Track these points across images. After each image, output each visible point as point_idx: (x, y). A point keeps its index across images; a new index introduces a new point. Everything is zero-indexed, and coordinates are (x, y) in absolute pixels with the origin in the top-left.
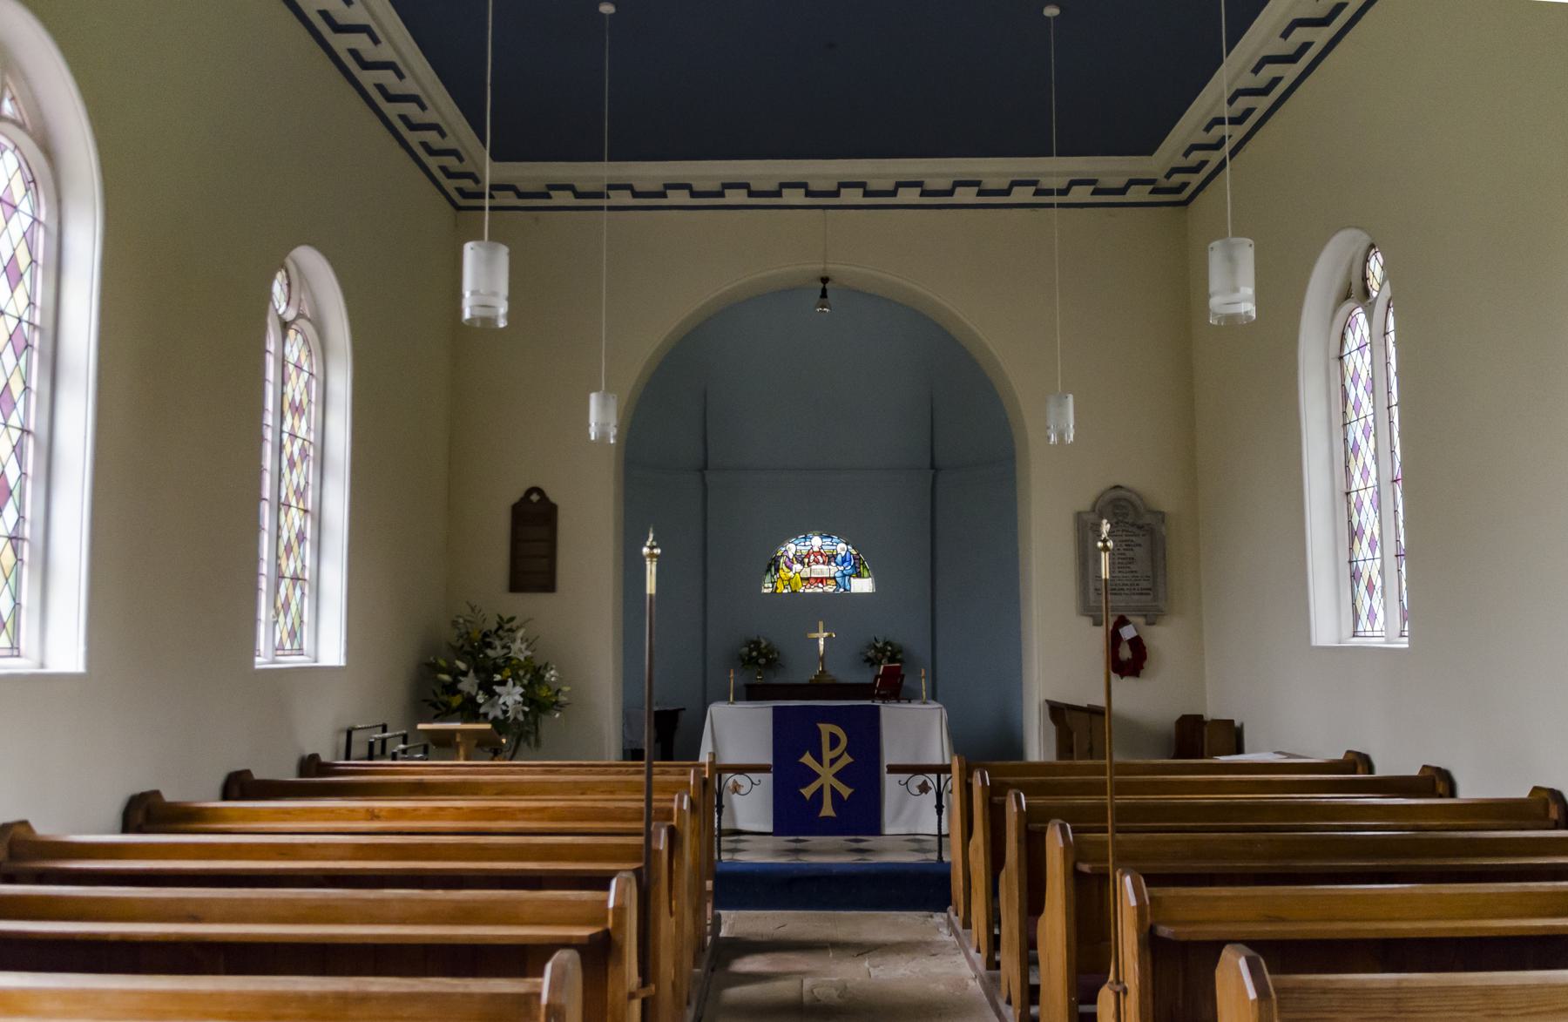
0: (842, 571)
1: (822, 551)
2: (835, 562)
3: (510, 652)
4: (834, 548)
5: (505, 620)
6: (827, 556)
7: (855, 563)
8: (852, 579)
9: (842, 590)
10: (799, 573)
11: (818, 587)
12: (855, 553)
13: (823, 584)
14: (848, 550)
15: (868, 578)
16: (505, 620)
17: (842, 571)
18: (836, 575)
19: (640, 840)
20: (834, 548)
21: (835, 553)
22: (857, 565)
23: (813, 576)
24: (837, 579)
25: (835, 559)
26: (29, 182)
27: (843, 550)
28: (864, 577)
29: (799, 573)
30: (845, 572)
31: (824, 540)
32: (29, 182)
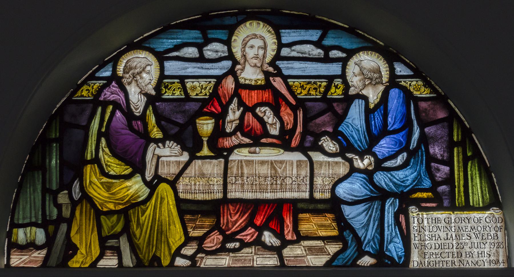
0: (369, 174)
1: (278, 83)
2: (335, 135)
3: (365, 98)
4: (335, 69)
5: (157, 148)
6: (301, 103)
7: (424, 139)
8: (413, 211)
9: (367, 261)
10: (173, 184)
11: (258, 242)
12: (424, 92)
13: (279, 234)
14: (393, 78)
15: (485, 208)
16: (157, 148)
17: (369, 174)
18: (342, 190)
19: (285, 40)
20: (335, 69)
21: (336, 93)
22: (436, 150)
23: (234, 194)
24: (348, 211)
25: (341, 118)
26: (417, 237)
27: (375, 82)
28: (468, 207)
29: (173, 184)
30: (381, 178)
31: (289, 36)
32: (417, 237)
